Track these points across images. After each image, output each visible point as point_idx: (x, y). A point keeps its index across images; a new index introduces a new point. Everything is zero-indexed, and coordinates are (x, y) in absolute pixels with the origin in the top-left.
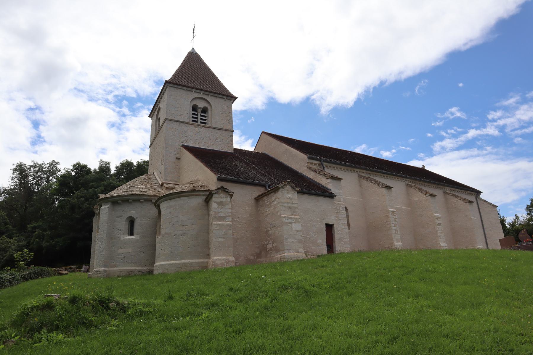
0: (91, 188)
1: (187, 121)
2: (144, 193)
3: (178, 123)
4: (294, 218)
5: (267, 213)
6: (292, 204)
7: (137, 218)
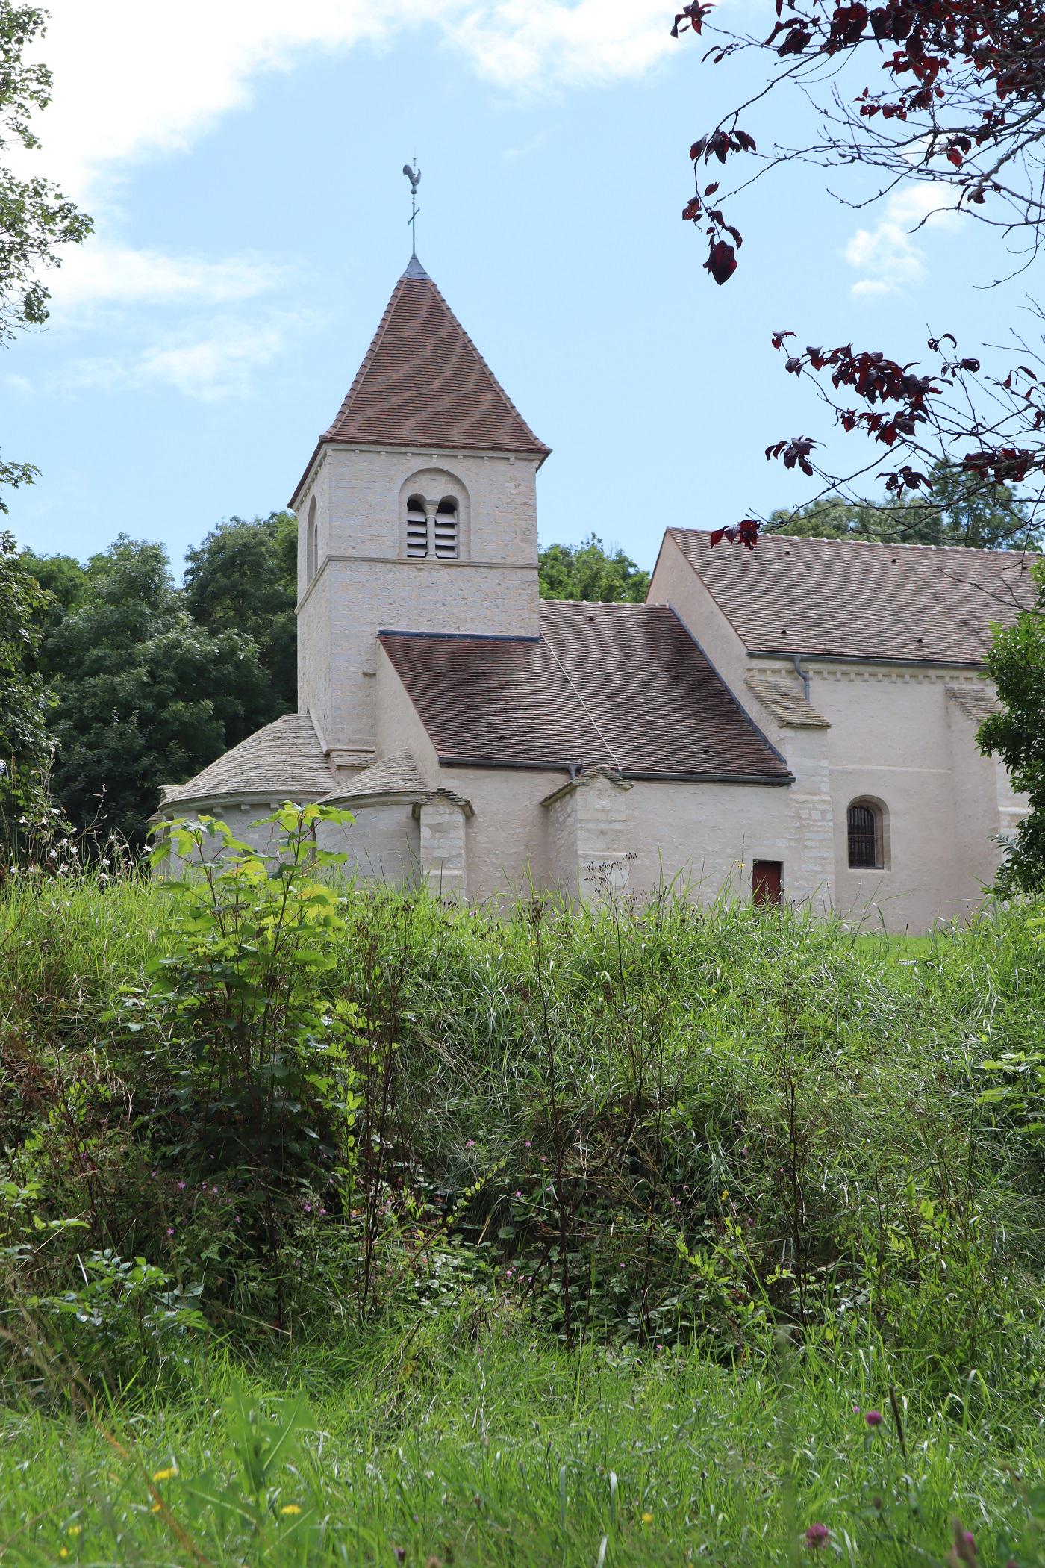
0: (95, 673)
1: (392, 554)
2: (278, 787)
3: (366, 566)
5: (562, 841)
6: (610, 822)
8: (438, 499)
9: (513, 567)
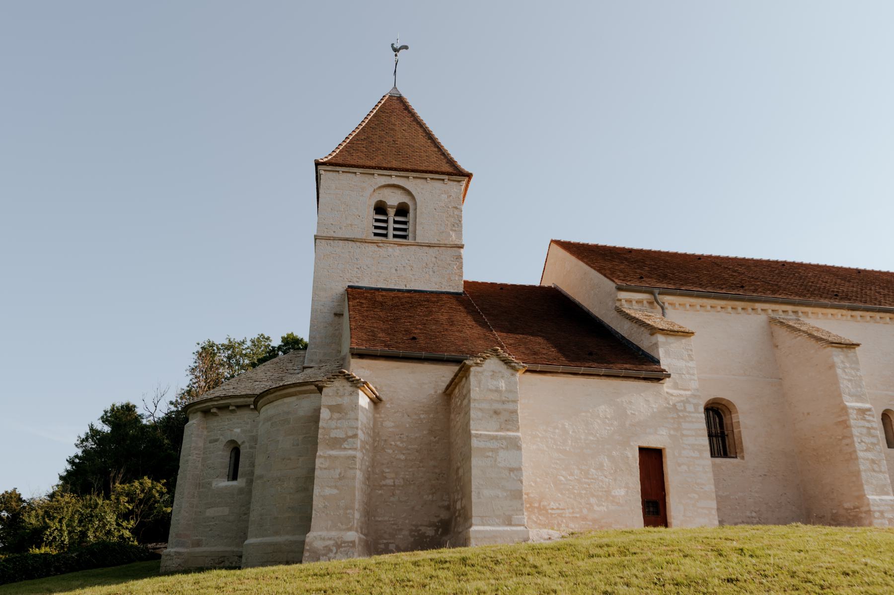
4: (502, 438)
6: (503, 402)
7: (243, 442)
8: (396, 204)
9: (446, 246)
